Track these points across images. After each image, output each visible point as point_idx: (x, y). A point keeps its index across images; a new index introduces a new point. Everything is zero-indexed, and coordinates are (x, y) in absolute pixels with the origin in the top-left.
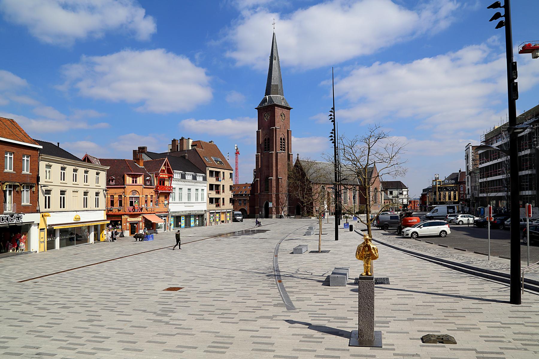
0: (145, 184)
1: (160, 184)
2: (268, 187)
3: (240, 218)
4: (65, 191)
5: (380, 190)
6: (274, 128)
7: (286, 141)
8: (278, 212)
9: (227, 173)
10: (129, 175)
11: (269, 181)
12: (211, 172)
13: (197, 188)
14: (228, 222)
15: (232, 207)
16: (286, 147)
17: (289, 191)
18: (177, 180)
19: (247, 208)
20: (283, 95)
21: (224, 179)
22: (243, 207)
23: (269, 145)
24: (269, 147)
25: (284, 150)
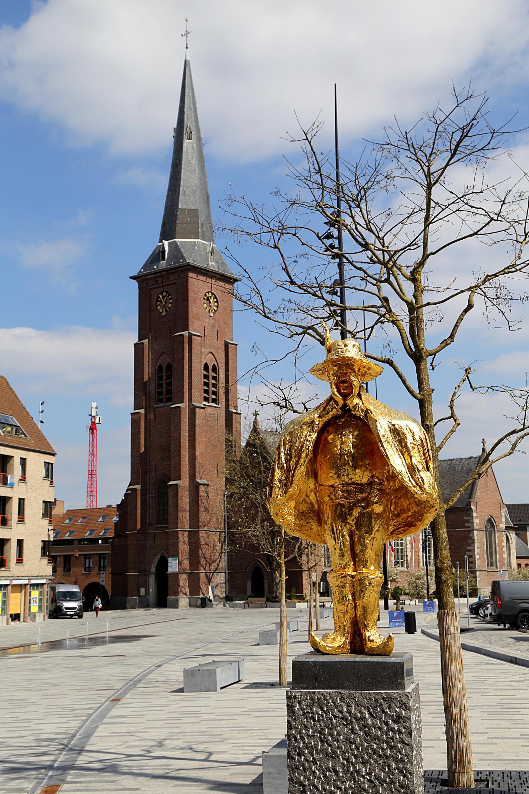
2: (166, 512)
3: (75, 604)
5: (503, 526)
6: (185, 333)
8: (195, 589)
9: (36, 462)
11: (171, 493)
14: (33, 617)
15: (48, 570)
16: (222, 392)
17: (230, 525)
19: (104, 579)
20: (211, 239)
21: (23, 479)
22: (95, 580)
23: (169, 384)
24: (169, 392)
25: (214, 401)
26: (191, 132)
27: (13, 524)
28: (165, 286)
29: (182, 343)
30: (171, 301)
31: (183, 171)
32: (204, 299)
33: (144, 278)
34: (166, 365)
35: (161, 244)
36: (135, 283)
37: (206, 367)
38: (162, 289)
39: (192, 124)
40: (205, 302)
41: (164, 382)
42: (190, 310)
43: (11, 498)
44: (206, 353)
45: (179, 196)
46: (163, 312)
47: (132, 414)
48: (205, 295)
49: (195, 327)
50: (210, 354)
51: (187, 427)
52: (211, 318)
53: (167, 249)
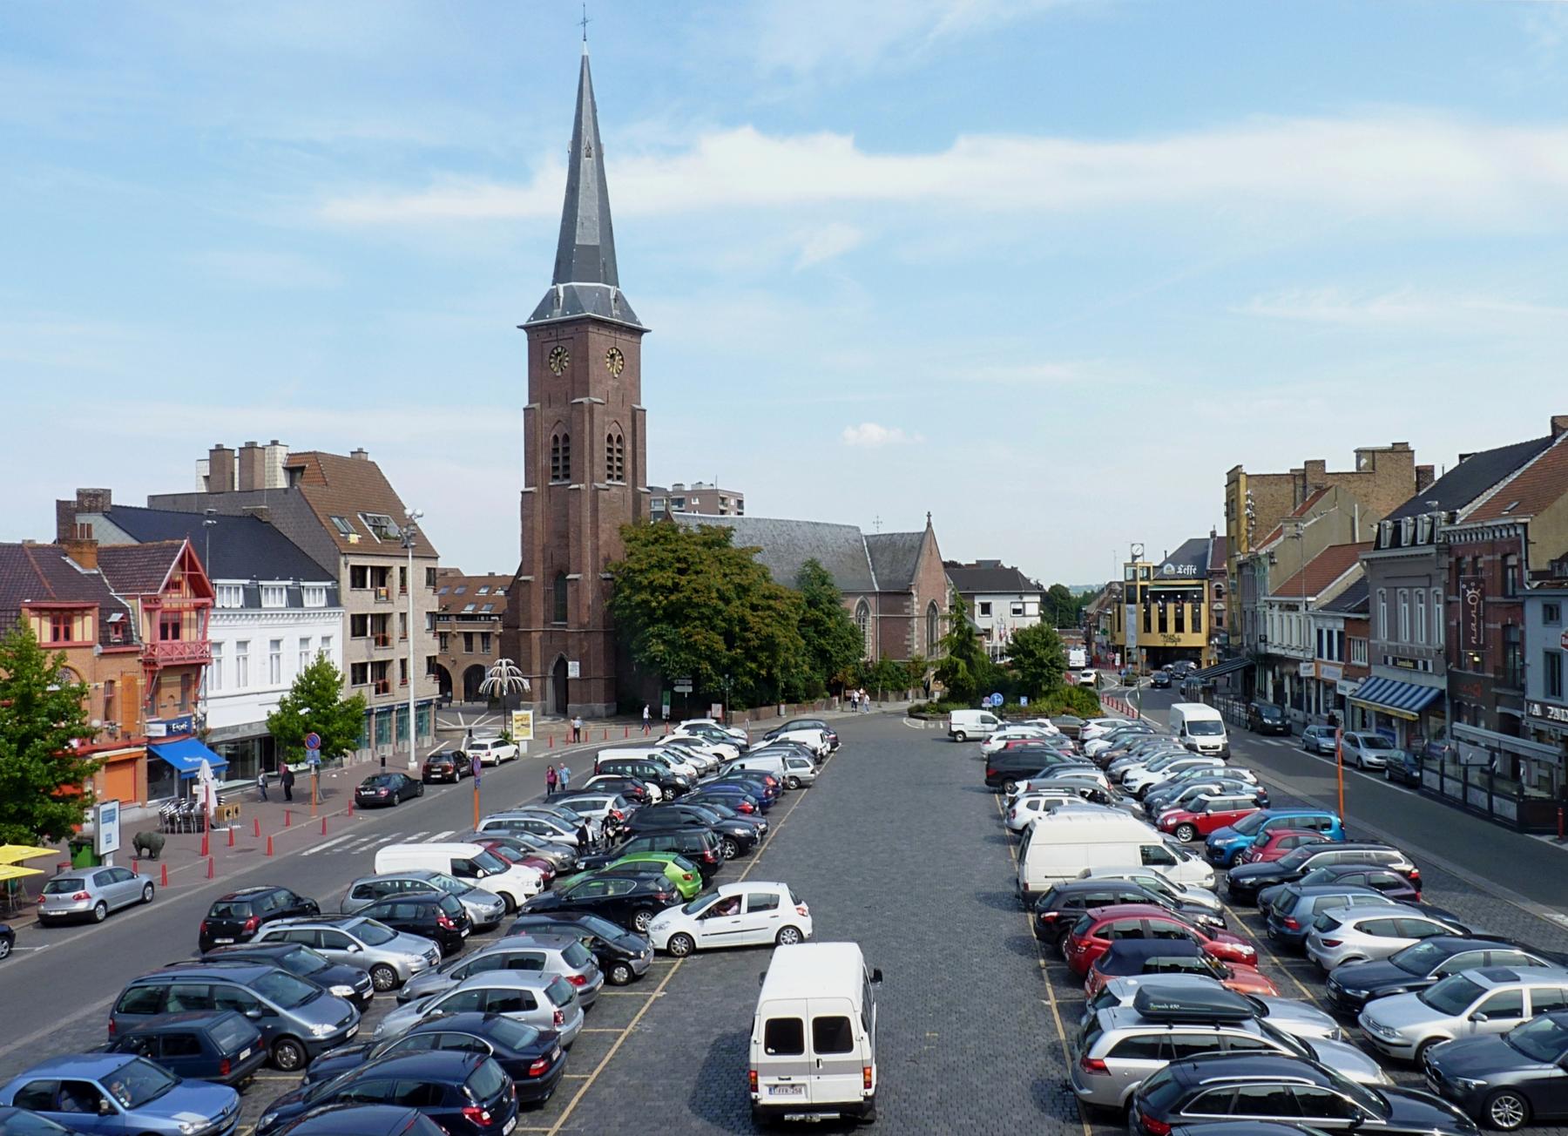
0: (104, 641)
1: (164, 636)
7: (629, 448)
10: (40, 611)
11: (570, 589)
12: (358, 576)
13: (305, 633)
16: (629, 466)
18: (229, 612)
23: (566, 458)
24: (567, 467)
25: (619, 478)
29: (583, 412)
36: (524, 334)
37: (610, 438)
41: (560, 455)
53: (561, 294)
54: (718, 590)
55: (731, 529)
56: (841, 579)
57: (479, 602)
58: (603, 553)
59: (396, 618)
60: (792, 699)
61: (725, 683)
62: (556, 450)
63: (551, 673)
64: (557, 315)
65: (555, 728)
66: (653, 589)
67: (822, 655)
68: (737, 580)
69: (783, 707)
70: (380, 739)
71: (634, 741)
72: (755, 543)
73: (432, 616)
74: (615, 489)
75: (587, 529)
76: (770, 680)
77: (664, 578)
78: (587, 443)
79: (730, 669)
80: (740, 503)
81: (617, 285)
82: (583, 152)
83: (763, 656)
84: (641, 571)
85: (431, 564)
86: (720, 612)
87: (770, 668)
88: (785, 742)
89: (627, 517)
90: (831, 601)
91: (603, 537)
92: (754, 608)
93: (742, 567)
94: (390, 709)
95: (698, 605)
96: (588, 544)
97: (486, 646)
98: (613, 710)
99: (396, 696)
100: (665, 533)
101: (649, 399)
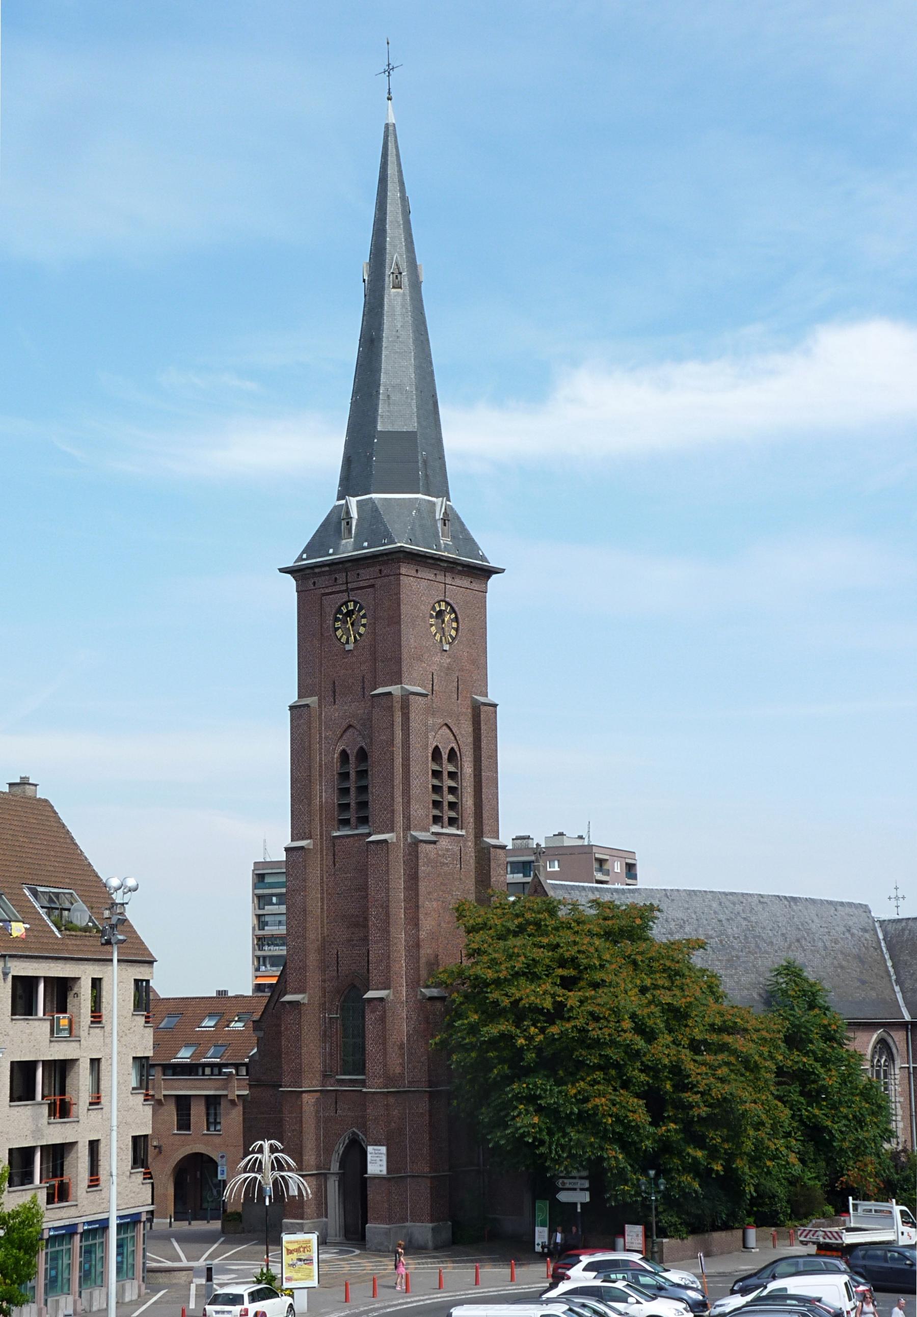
4: (89, 1187)
7: (468, 769)
16: (468, 802)
23: (363, 790)
25: (452, 822)
26: (401, 273)
27: (80, 1111)
28: (353, 590)
29: (390, 708)
30: (364, 621)
31: (384, 353)
32: (431, 616)
33: (308, 571)
34: (355, 751)
35: (343, 502)
36: (290, 582)
38: (344, 597)
39: (401, 256)
40: (432, 621)
41: (352, 784)
42: (403, 643)
43: (77, 1060)
44: (438, 727)
45: (377, 405)
46: (347, 642)
47: (287, 850)
48: (433, 608)
49: (415, 675)
50: (445, 727)
51: (402, 882)
52: (445, 654)
53: (354, 514)
54: (633, 1016)
55: (651, 908)
56: (843, 996)
57: (199, 1042)
58: (426, 951)
59: (84, 1068)
60: (766, 1219)
61: (644, 1184)
62: (344, 776)
63: (335, 1167)
64: (347, 548)
65: (346, 1268)
66: (519, 1013)
67: (815, 1134)
68: (666, 998)
69: (752, 1233)
70: (52, 1284)
71: (492, 1291)
72: (689, 932)
73: (141, 1063)
74: (445, 843)
75: (399, 912)
76: (730, 1183)
77: (538, 994)
78: (398, 761)
79: (655, 1160)
80: (630, 869)
81: (444, 493)
82: (389, 280)
83: (715, 1137)
84: (497, 982)
85: (140, 972)
86: (636, 1055)
87: (730, 1158)
88: (780, 1296)
89: (465, 888)
90: (829, 1037)
91: (427, 924)
92: (695, 1047)
93: (673, 974)
94: (70, 1231)
95: (597, 1043)
96: (400, 936)
97: (213, 1121)
98: (446, 1235)
99: (83, 1208)
100: (536, 916)
101: (505, 683)
